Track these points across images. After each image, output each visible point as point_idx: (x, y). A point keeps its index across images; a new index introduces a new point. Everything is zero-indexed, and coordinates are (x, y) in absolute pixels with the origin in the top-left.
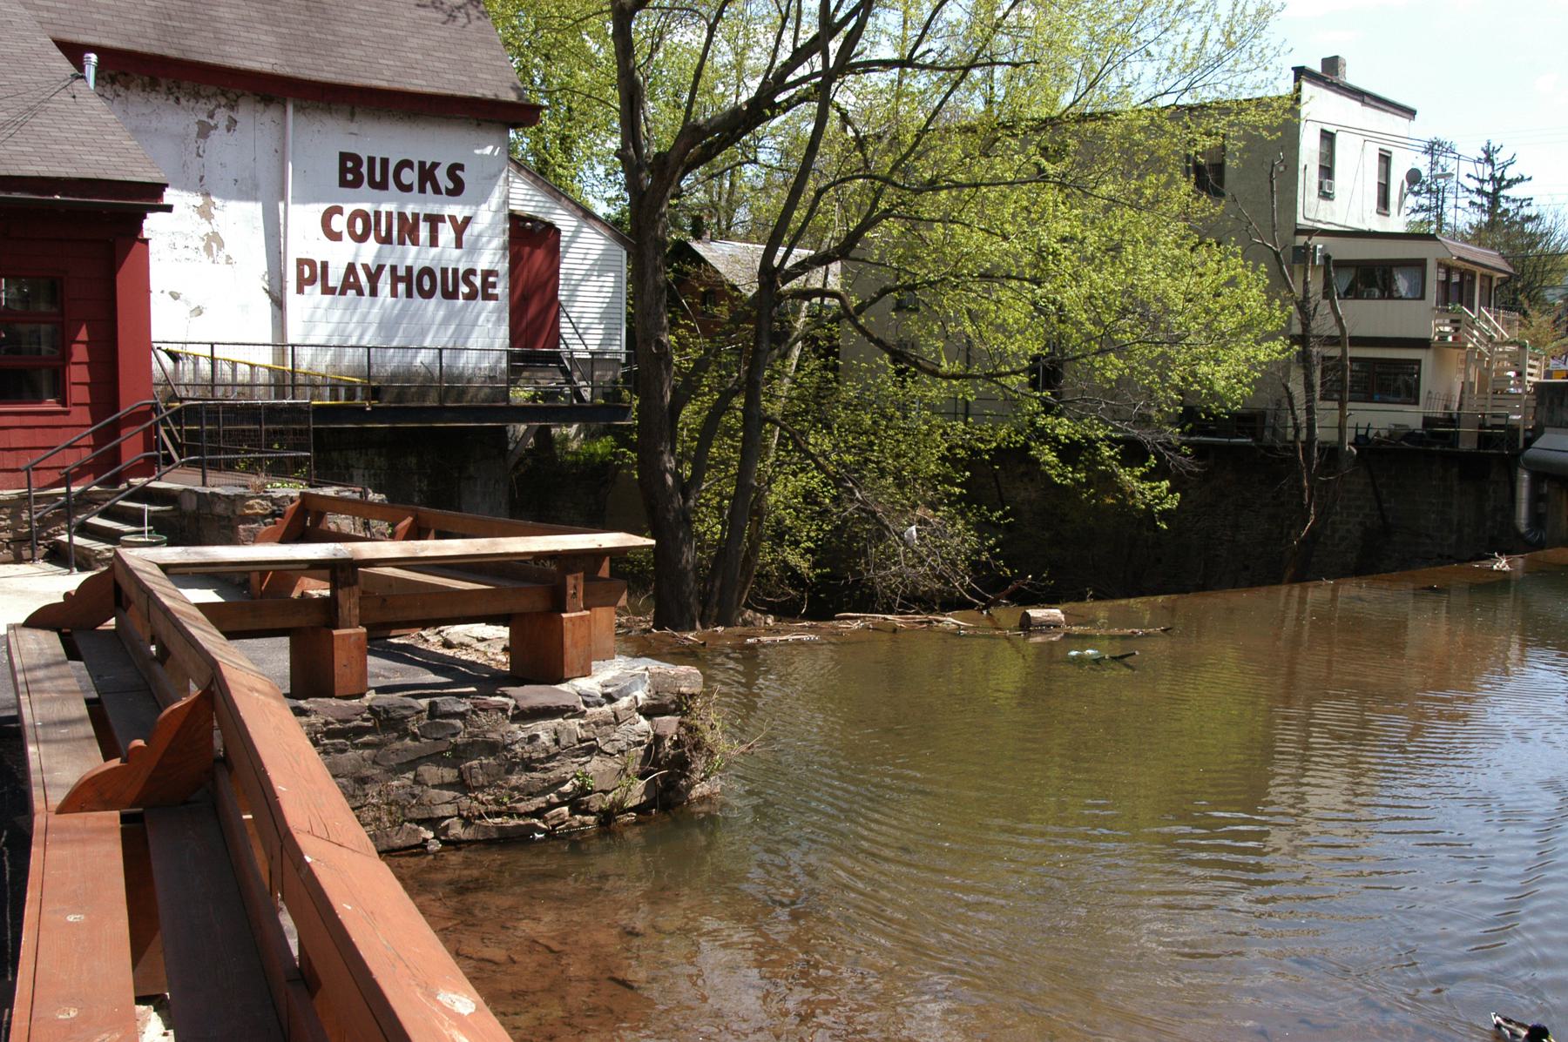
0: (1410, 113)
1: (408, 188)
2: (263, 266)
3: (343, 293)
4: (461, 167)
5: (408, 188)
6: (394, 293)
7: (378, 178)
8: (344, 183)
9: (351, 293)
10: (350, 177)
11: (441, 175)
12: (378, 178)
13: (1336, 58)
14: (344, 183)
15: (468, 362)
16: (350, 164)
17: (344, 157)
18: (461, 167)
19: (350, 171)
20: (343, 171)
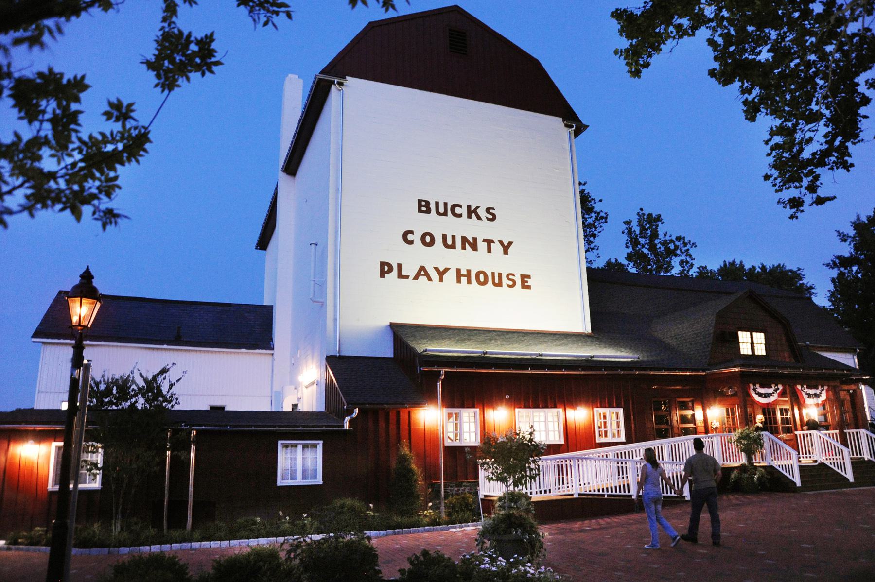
0: (835, 197)
1: (460, 216)
2: (267, 208)
3: (416, 278)
4: (529, 277)
5: (460, 216)
6: (454, 237)
7: (497, 281)
8: (420, 211)
9: (423, 279)
10: (424, 209)
11: (482, 212)
12: (497, 281)
13: (755, 121)
14: (420, 211)
15: (304, 408)
16: (424, 209)
17: (420, 201)
18: (529, 277)
19: (423, 206)
20: (420, 205)
